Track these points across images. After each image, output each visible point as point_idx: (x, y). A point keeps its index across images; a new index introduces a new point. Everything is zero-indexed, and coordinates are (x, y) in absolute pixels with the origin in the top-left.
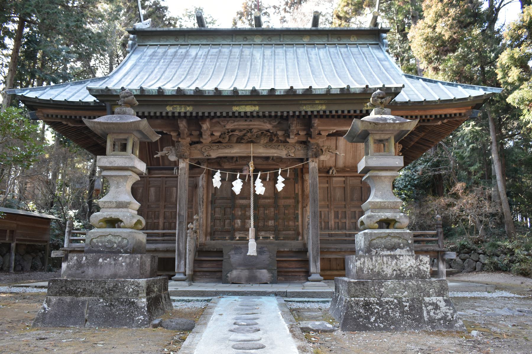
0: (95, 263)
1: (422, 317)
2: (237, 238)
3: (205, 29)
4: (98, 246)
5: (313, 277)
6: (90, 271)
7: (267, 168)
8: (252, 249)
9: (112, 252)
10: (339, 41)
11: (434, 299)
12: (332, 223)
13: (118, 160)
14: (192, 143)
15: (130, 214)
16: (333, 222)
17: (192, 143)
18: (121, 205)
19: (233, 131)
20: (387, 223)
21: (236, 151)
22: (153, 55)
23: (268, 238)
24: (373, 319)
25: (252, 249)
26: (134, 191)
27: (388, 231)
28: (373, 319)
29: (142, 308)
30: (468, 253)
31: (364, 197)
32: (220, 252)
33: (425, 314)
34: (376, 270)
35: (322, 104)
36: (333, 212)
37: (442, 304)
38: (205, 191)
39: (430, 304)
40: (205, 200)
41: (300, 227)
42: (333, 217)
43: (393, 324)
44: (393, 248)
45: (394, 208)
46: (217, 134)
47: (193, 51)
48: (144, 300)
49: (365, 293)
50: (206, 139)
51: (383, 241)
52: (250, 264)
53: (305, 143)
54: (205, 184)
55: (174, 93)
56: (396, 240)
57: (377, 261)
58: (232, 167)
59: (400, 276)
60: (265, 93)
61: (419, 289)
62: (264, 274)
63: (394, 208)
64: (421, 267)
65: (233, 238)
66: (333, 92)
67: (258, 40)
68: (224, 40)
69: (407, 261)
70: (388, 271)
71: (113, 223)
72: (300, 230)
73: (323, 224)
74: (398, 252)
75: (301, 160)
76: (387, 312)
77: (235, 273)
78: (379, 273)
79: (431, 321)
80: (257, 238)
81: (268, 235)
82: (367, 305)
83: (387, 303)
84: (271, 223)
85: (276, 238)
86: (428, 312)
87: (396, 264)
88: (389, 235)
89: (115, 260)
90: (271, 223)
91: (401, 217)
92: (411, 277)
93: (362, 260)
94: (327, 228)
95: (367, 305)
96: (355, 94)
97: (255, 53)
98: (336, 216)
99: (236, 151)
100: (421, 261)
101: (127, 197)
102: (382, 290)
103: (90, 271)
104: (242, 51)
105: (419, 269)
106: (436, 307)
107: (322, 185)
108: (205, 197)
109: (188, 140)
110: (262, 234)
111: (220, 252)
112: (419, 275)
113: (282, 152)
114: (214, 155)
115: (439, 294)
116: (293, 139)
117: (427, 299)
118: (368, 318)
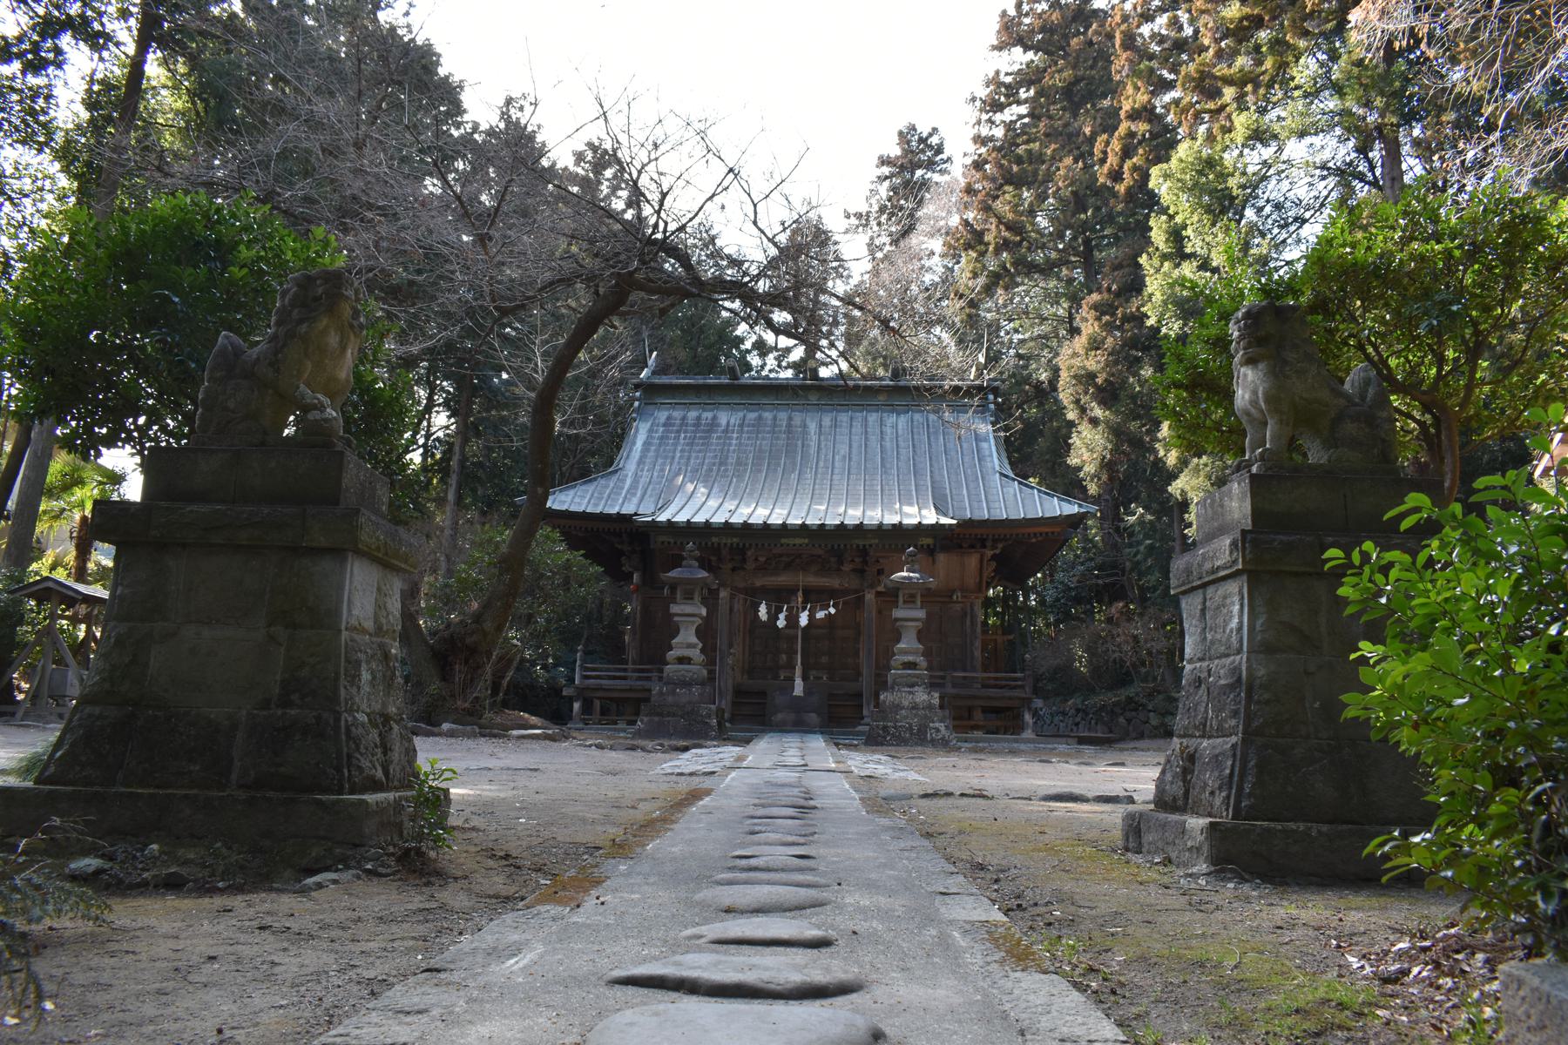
0: (674, 692)
6: (670, 699)
7: (815, 597)
8: (799, 688)
9: (686, 684)
13: (688, 609)
14: (734, 569)
15: (695, 654)
17: (734, 569)
18: (690, 646)
19: (781, 556)
20: (911, 665)
21: (783, 579)
22: (668, 423)
25: (799, 688)
26: (698, 633)
30: (1136, 710)
31: (898, 641)
32: (763, 694)
44: (912, 686)
45: (915, 652)
46: (762, 559)
47: (724, 417)
49: (884, 719)
50: (750, 565)
52: (797, 706)
53: (861, 572)
58: (779, 597)
59: (915, 707)
62: (813, 718)
63: (915, 652)
65: (776, 677)
67: (813, 399)
69: (921, 696)
70: (906, 703)
71: (682, 660)
75: (856, 591)
77: (780, 716)
79: (933, 740)
80: (804, 678)
82: (885, 728)
84: (824, 659)
85: (830, 679)
90: (824, 659)
95: (885, 728)
97: (808, 421)
99: (783, 579)
101: (694, 640)
103: (670, 699)
104: (790, 419)
106: (938, 730)
109: (730, 566)
110: (813, 673)
111: (763, 694)
112: (930, 707)
113: (835, 582)
114: (758, 583)
116: (847, 567)
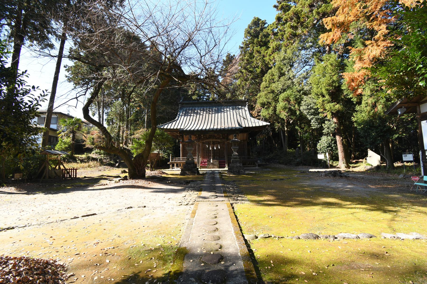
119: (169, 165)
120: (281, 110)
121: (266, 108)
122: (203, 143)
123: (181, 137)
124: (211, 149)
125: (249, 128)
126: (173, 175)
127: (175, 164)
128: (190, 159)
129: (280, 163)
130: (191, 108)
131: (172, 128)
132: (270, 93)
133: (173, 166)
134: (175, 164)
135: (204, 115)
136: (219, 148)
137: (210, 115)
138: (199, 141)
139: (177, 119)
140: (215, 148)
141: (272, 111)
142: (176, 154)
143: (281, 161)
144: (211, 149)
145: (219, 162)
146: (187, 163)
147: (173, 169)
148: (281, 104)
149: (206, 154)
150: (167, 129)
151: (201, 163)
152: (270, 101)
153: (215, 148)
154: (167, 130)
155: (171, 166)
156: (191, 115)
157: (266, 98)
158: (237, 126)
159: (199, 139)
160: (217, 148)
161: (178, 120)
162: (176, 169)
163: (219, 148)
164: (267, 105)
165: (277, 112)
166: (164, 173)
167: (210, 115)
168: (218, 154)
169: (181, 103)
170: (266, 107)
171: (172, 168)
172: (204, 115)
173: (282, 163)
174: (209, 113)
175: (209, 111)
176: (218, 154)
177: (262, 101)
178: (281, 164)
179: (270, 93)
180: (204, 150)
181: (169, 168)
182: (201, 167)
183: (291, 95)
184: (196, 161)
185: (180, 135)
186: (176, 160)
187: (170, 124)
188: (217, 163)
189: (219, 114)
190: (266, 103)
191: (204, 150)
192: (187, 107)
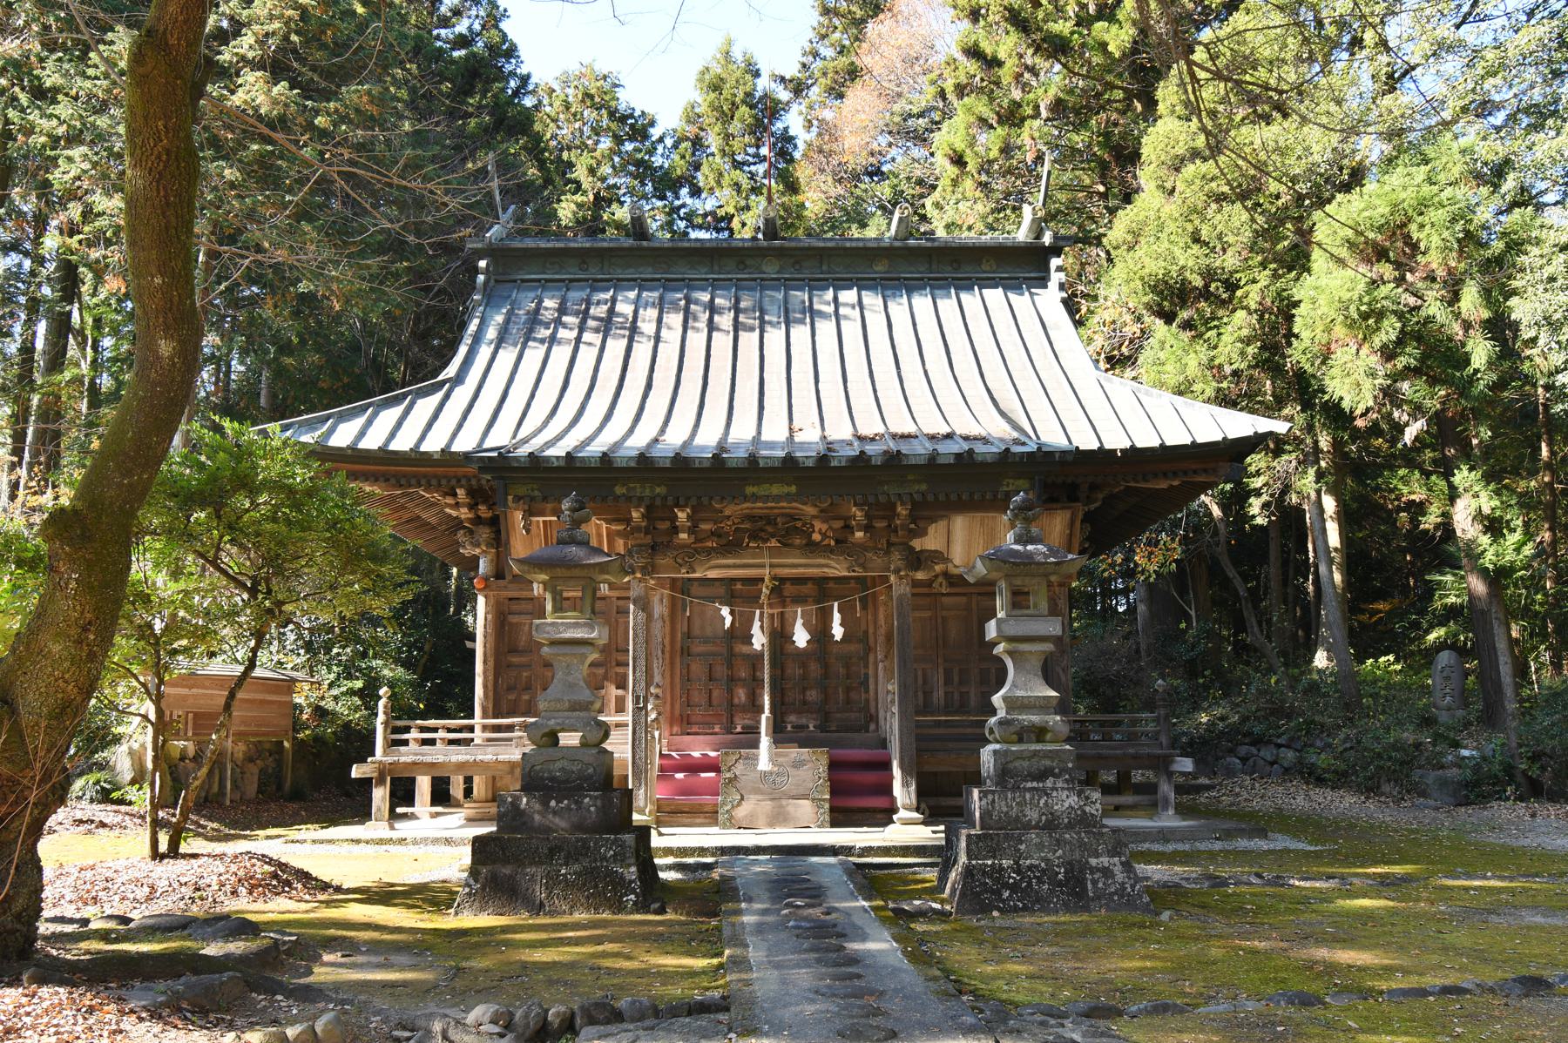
1: (1085, 889)
2: (739, 729)
3: (651, 244)
4: (542, 779)
5: (903, 814)
10: (956, 270)
11: (1105, 861)
12: (939, 695)
16: (941, 693)
23: (804, 727)
24: (1006, 894)
27: (1038, 747)
28: (1006, 894)
29: (631, 882)
33: (1090, 886)
34: (1013, 813)
35: (919, 482)
36: (941, 670)
37: (1118, 869)
38: (668, 629)
39: (1098, 870)
40: (668, 648)
41: (872, 704)
42: (941, 682)
43: (1037, 901)
44: (1042, 775)
48: (633, 869)
51: (1026, 764)
54: (666, 612)
55: (633, 464)
56: (1048, 763)
57: (1014, 799)
59: (1051, 825)
60: (810, 463)
61: (1082, 845)
64: (1087, 809)
66: (941, 461)
68: (693, 267)
69: (1066, 801)
70: (1032, 815)
72: (873, 711)
73: (920, 695)
74: (1049, 783)
76: (1030, 884)
78: (1017, 819)
81: (804, 721)
83: (1030, 868)
86: (1095, 882)
87: (1046, 803)
88: (1035, 753)
89: (576, 802)
91: (1056, 723)
92: (1070, 826)
93: (990, 797)
94: (926, 708)
96: (984, 464)
98: (948, 681)
100: (1087, 798)
102: (1023, 847)
105: (1084, 812)
107: (918, 614)
108: (667, 641)
115: (1113, 853)
117: (1093, 861)
118: (999, 893)
119: (366, 784)
120: (1340, 331)
121: (1187, 325)
122: (682, 588)
123: (485, 533)
124: (759, 640)
125: (1102, 456)
126: (384, 895)
127: (424, 785)
128: (569, 739)
129: (1316, 778)
130: (575, 295)
131: (403, 444)
132: (1220, 198)
133: (403, 793)
134: (424, 785)
135: (672, 336)
136: (838, 632)
137: (722, 342)
138: (650, 569)
139: (451, 371)
140: (801, 638)
141: (1248, 341)
142: (441, 687)
143: (1322, 760)
144: (759, 640)
145: (834, 766)
146: (534, 780)
147: (404, 829)
148: (1329, 288)
149: (714, 689)
150: (384, 457)
151: (666, 772)
152: (1230, 261)
153: (801, 638)
154: (356, 461)
155: (380, 795)
156: (553, 340)
157: (1196, 238)
158: (998, 429)
159: (655, 542)
160: (820, 633)
161: (459, 379)
162: (425, 820)
163: (838, 632)
164: (1205, 293)
165: (1298, 355)
166: (284, 878)
167: (722, 342)
168: (813, 695)
169: (492, 252)
170: (1184, 315)
171: (394, 817)
172: (672, 336)
173: (1338, 780)
174: (712, 327)
175: (712, 309)
176: (813, 695)
177: (1155, 268)
178: (1320, 781)
179: (1220, 198)
180: (686, 652)
181: (362, 813)
182: (670, 814)
183: (1423, 206)
184: (620, 747)
185: (478, 520)
186: (429, 748)
187: (390, 416)
188: (810, 767)
189: (800, 333)
190: (1198, 282)
191: (686, 652)
192: (545, 285)
